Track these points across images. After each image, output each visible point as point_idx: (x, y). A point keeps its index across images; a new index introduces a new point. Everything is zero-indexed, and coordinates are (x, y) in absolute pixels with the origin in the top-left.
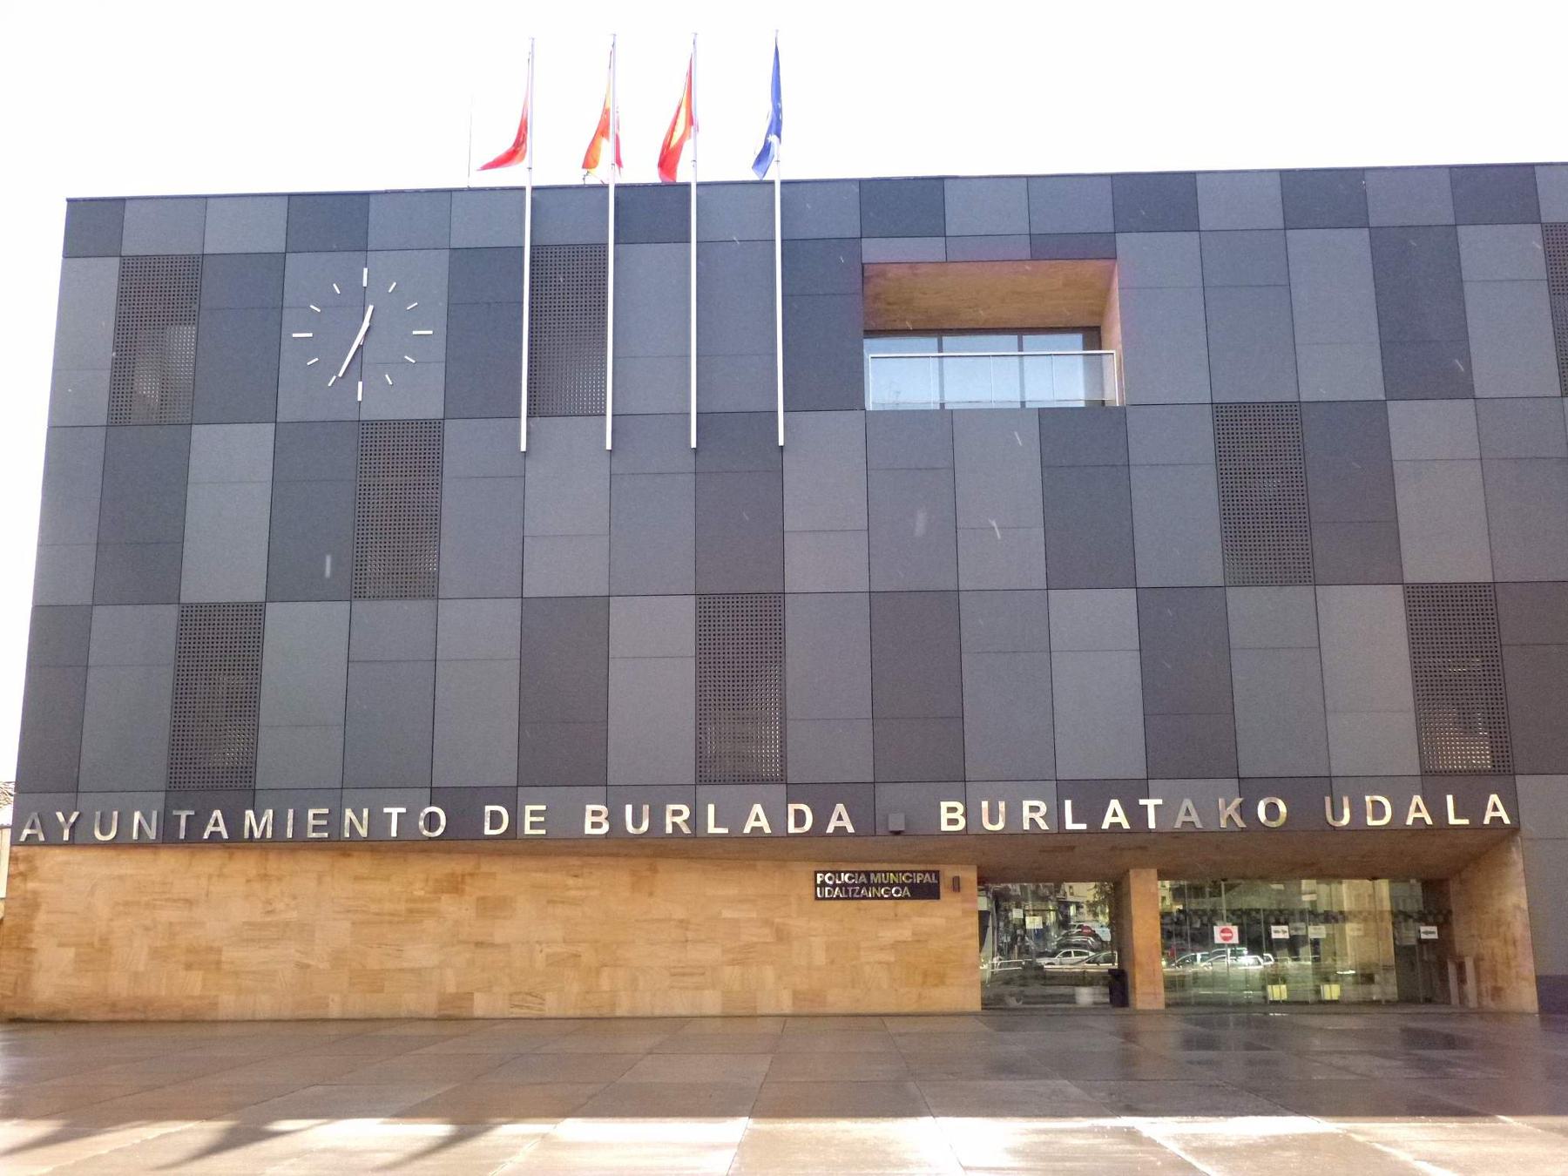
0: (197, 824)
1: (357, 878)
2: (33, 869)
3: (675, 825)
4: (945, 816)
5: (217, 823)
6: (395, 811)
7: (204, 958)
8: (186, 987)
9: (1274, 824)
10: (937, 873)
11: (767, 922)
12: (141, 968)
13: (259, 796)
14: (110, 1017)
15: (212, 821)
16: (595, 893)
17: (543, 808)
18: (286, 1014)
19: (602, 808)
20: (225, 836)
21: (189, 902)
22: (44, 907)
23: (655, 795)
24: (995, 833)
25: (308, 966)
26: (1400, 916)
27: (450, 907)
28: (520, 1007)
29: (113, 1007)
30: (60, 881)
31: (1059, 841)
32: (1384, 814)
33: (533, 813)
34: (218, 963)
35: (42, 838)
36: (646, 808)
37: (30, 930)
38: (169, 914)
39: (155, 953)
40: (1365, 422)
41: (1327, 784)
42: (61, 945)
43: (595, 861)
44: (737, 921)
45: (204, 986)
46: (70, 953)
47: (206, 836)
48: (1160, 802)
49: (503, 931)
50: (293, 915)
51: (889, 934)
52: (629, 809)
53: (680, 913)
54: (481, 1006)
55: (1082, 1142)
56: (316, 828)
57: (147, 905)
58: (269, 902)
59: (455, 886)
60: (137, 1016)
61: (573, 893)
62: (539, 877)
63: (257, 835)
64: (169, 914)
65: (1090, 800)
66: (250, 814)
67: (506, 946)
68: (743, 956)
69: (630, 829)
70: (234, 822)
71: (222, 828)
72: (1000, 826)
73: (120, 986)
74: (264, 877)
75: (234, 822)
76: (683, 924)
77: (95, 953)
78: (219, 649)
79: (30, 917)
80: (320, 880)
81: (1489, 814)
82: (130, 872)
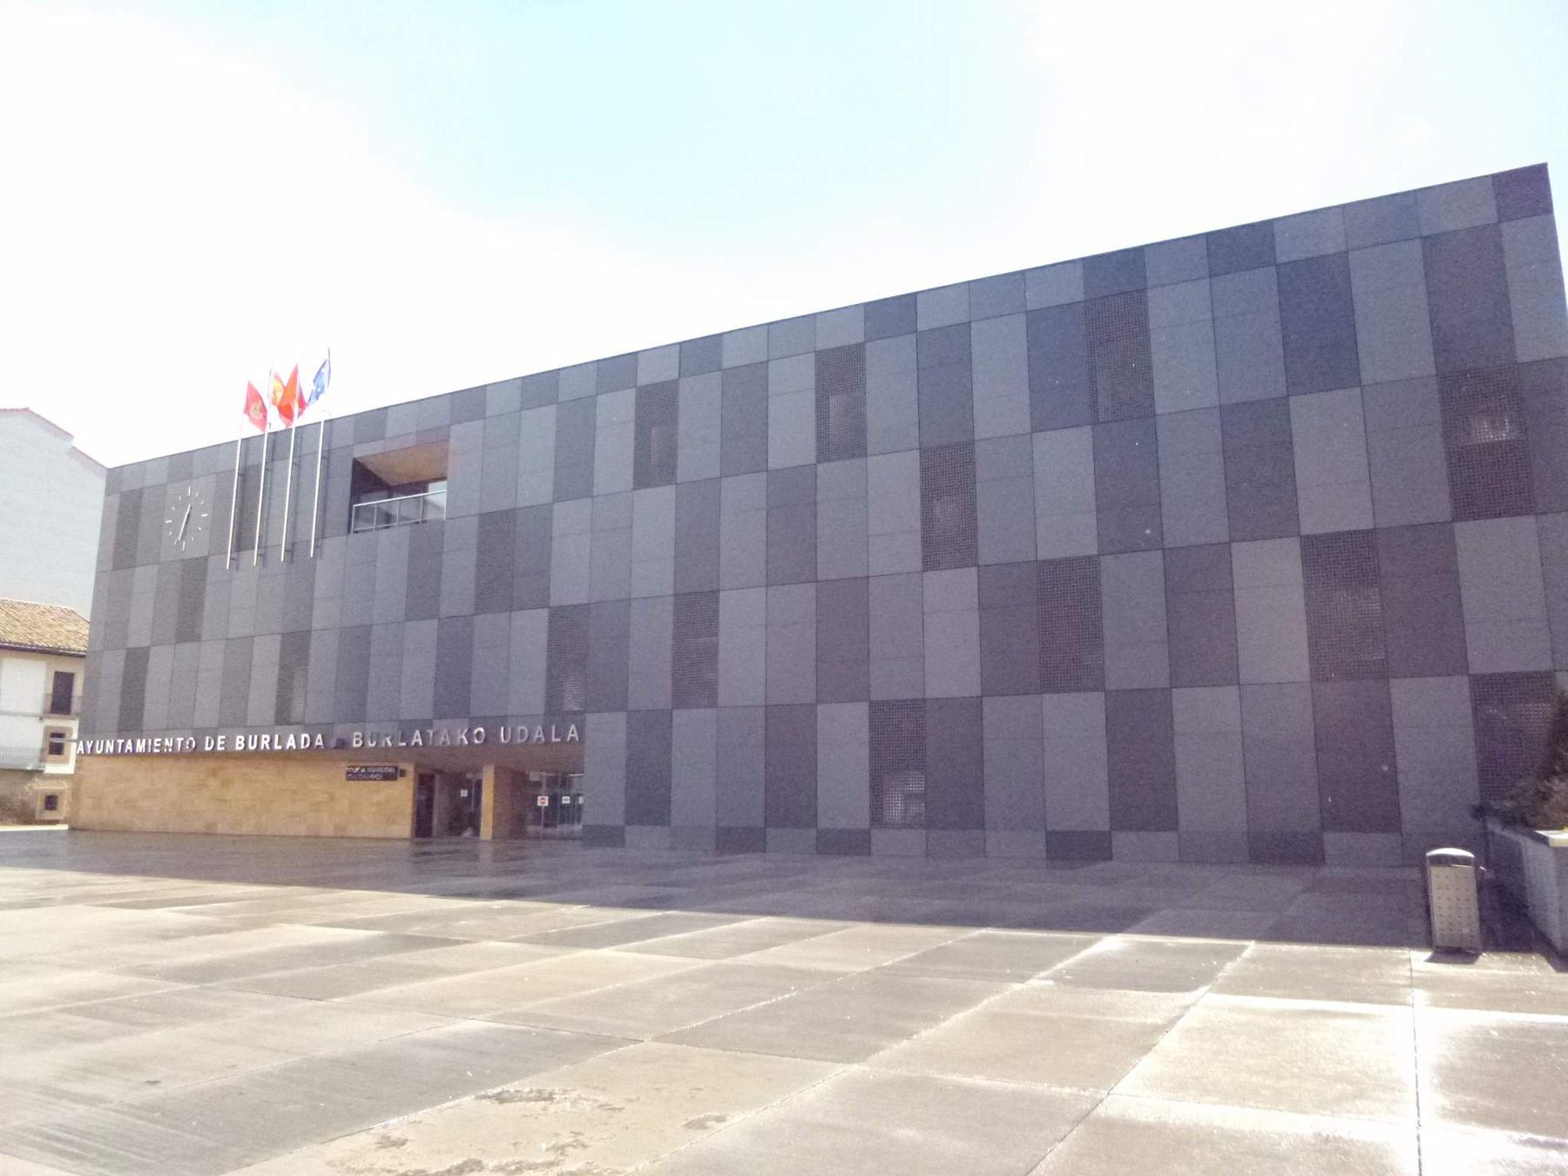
6: (180, 740)
8: (123, 817)
23: (258, 730)
27: (213, 783)
31: (396, 748)
40: (543, 514)
41: (503, 720)
51: (376, 798)
54: (221, 828)
55: (1011, 1085)
59: (214, 773)
65: (199, 734)
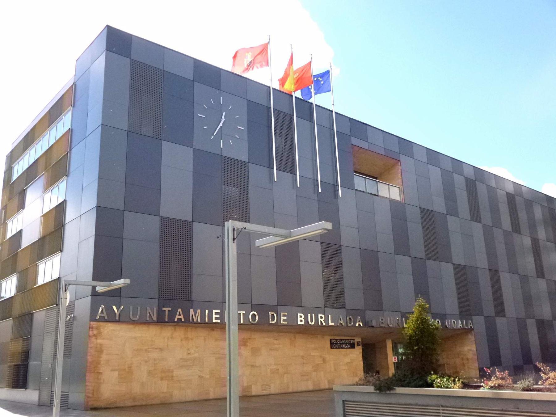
0: (172, 314)
1: (217, 340)
2: (100, 333)
3: (321, 321)
4: (299, 319)
5: (179, 315)
7: (167, 375)
9: (253, 323)
10: (354, 340)
11: (321, 357)
12: (144, 380)
13: (194, 303)
14: (133, 404)
15: (178, 313)
16: (281, 346)
17: (309, 315)
18: (196, 399)
19: (323, 316)
20: (183, 320)
21: (161, 350)
22: (105, 351)
24: (303, 325)
25: (203, 377)
26: (431, 355)
28: (265, 390)
29: (134, 399)
30: (112, 339)
32: (274, 321)
33: (216, 313)
34: (172, 377)
35: (106, 318)
36: (313, 315)
37: (99, 363)
38: (155, 355)
39: (150, 373)
42: (112, 370)
43: (282, 334)
44: (314, 356)
45: (168, 388)
46: (116, 373)
47: (176, 320)
48: (244, 312)
49: (259, 361)
50: (196, 355)
52: (309, 315)
53: (301, 353)
56: (216, 318)
57: (146, 350)
58: (188, 350)
60: (144, 403)
61: (276, 346)
62: (271, 340)
63: (195, 320)
64: (155, 355)
66: (192, 311)
67: (260, 366)
68: (316, 368)
69: (310, 323)
70: (186, 314)
71: (182, 317)
72: (313, 323)
73: (136, 389)
74: (187, 339)
75: (186, 314)
76: (303, 357)
77: (126, 373)
78: (176, 239)
79: (99, 357)
80: (205, 340)
81: (177, 317)
82: (139, 335)
